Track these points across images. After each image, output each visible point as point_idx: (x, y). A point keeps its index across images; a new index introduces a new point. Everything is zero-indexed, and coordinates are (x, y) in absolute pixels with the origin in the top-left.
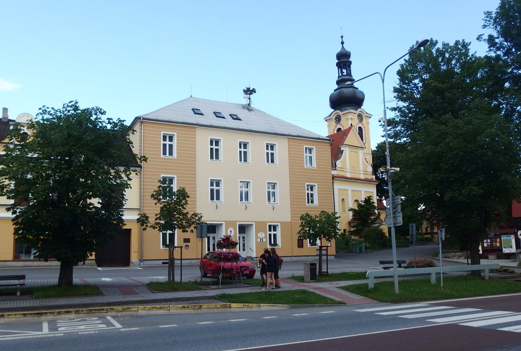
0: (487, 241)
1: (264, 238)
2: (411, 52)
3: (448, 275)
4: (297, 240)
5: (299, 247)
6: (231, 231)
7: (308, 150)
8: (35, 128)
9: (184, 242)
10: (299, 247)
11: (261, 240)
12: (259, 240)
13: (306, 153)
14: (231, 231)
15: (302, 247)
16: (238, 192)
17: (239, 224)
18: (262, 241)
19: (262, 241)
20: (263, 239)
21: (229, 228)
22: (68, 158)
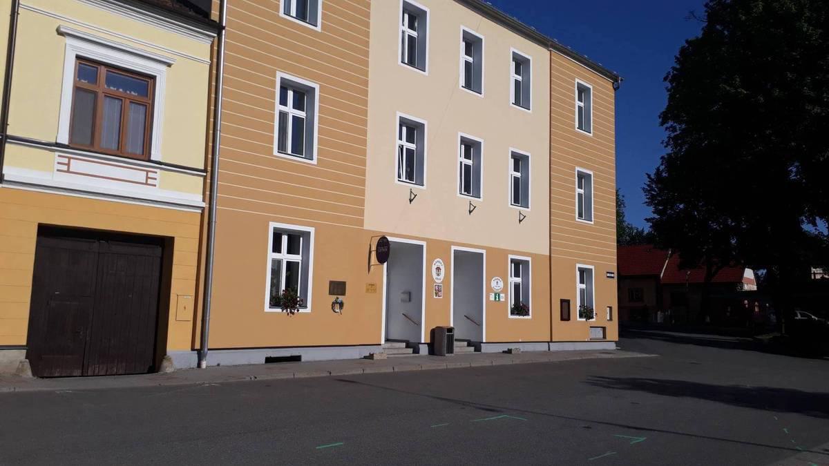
0: (815, 277)
1: (502, 292)
2: (103, 70)
3: (517, 362)
4: (559, 302)
5: (562, 319)
6: (438, 269)
7: (290, 94)
8: (144, 100)
9: (331, 293)
10: (562, 319)
11: (496, 298)
12: (492, 298)
13: (283, 101)
14: (438, 269)
15: (568, 319)
16: (527, 151)
17: (275, 229)
18: (497, 299)
19: (497, 299)
20: (501, 295)
21: (435, 259)
22: (718, 27)
